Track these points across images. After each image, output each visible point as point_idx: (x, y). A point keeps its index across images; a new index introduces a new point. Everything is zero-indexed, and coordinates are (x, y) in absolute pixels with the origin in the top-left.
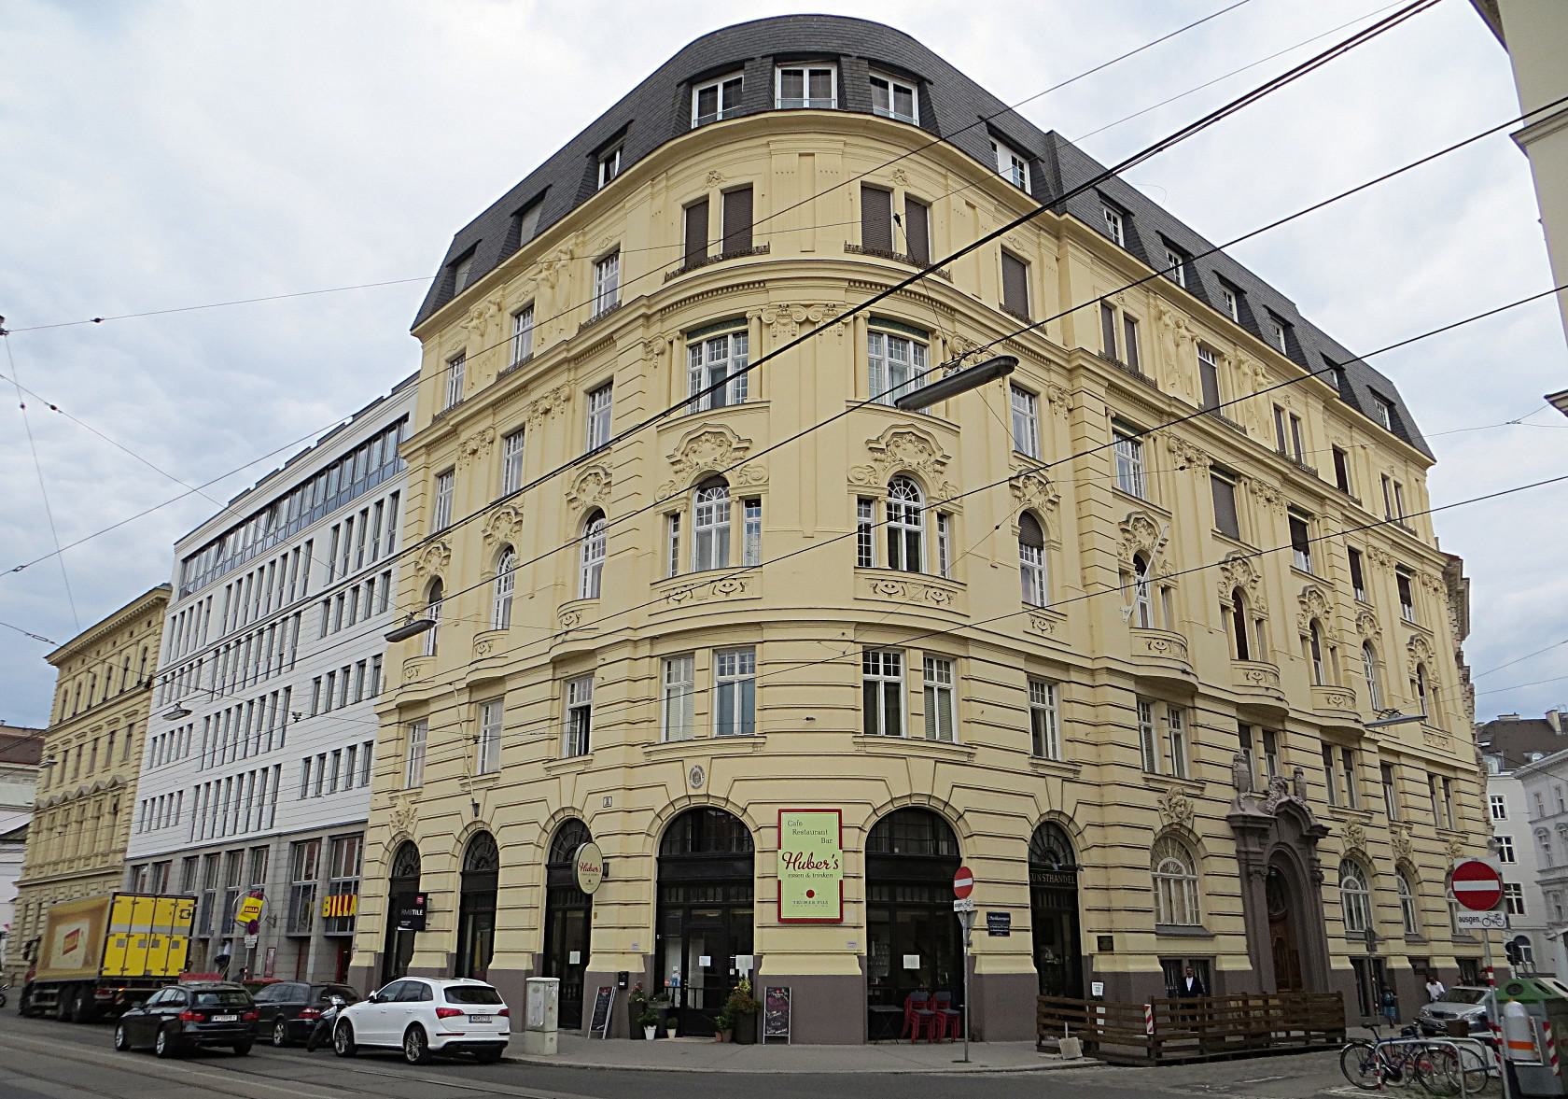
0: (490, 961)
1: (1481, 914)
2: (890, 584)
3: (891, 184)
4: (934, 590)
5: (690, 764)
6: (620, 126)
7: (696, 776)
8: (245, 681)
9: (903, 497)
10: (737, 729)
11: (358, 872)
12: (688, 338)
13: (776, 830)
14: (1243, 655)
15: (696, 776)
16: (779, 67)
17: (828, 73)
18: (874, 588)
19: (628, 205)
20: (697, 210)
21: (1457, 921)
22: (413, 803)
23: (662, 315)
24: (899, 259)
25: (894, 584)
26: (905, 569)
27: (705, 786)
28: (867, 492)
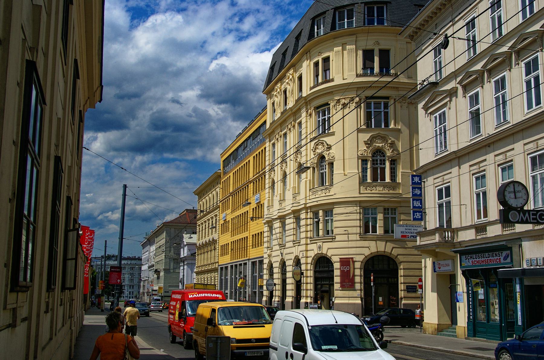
0: (285, 299)
6: (285, 49)
7: (320, 247)
8: (306, 197)
9: (379, 157)
11: (263, 272)
12: (317, 109)
13: (74, 261)
15: (320, 247)
19: (334, 42)
20: (316, 64)
22: (271, 251)
23: (309, 102)
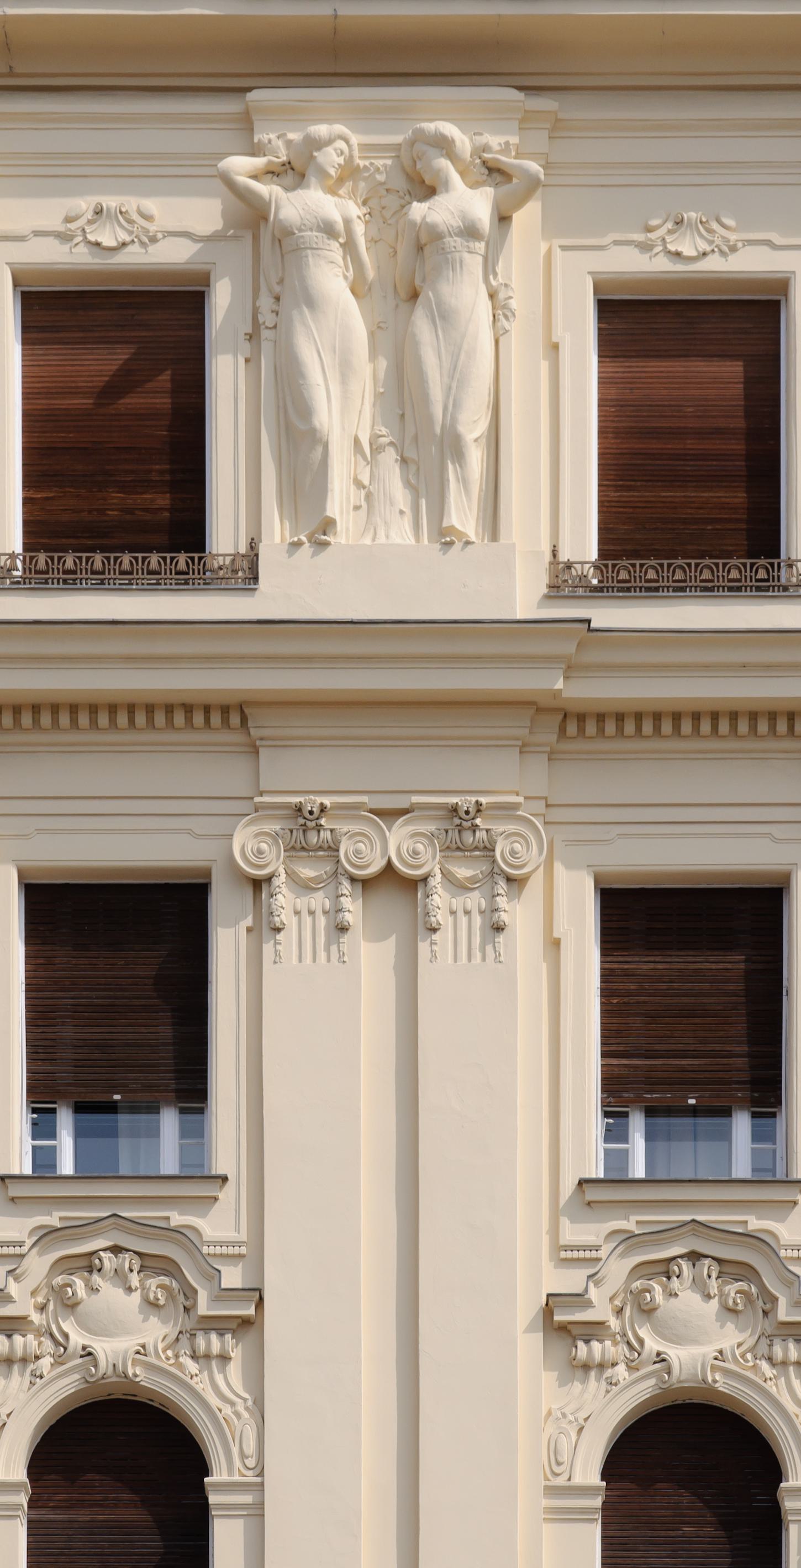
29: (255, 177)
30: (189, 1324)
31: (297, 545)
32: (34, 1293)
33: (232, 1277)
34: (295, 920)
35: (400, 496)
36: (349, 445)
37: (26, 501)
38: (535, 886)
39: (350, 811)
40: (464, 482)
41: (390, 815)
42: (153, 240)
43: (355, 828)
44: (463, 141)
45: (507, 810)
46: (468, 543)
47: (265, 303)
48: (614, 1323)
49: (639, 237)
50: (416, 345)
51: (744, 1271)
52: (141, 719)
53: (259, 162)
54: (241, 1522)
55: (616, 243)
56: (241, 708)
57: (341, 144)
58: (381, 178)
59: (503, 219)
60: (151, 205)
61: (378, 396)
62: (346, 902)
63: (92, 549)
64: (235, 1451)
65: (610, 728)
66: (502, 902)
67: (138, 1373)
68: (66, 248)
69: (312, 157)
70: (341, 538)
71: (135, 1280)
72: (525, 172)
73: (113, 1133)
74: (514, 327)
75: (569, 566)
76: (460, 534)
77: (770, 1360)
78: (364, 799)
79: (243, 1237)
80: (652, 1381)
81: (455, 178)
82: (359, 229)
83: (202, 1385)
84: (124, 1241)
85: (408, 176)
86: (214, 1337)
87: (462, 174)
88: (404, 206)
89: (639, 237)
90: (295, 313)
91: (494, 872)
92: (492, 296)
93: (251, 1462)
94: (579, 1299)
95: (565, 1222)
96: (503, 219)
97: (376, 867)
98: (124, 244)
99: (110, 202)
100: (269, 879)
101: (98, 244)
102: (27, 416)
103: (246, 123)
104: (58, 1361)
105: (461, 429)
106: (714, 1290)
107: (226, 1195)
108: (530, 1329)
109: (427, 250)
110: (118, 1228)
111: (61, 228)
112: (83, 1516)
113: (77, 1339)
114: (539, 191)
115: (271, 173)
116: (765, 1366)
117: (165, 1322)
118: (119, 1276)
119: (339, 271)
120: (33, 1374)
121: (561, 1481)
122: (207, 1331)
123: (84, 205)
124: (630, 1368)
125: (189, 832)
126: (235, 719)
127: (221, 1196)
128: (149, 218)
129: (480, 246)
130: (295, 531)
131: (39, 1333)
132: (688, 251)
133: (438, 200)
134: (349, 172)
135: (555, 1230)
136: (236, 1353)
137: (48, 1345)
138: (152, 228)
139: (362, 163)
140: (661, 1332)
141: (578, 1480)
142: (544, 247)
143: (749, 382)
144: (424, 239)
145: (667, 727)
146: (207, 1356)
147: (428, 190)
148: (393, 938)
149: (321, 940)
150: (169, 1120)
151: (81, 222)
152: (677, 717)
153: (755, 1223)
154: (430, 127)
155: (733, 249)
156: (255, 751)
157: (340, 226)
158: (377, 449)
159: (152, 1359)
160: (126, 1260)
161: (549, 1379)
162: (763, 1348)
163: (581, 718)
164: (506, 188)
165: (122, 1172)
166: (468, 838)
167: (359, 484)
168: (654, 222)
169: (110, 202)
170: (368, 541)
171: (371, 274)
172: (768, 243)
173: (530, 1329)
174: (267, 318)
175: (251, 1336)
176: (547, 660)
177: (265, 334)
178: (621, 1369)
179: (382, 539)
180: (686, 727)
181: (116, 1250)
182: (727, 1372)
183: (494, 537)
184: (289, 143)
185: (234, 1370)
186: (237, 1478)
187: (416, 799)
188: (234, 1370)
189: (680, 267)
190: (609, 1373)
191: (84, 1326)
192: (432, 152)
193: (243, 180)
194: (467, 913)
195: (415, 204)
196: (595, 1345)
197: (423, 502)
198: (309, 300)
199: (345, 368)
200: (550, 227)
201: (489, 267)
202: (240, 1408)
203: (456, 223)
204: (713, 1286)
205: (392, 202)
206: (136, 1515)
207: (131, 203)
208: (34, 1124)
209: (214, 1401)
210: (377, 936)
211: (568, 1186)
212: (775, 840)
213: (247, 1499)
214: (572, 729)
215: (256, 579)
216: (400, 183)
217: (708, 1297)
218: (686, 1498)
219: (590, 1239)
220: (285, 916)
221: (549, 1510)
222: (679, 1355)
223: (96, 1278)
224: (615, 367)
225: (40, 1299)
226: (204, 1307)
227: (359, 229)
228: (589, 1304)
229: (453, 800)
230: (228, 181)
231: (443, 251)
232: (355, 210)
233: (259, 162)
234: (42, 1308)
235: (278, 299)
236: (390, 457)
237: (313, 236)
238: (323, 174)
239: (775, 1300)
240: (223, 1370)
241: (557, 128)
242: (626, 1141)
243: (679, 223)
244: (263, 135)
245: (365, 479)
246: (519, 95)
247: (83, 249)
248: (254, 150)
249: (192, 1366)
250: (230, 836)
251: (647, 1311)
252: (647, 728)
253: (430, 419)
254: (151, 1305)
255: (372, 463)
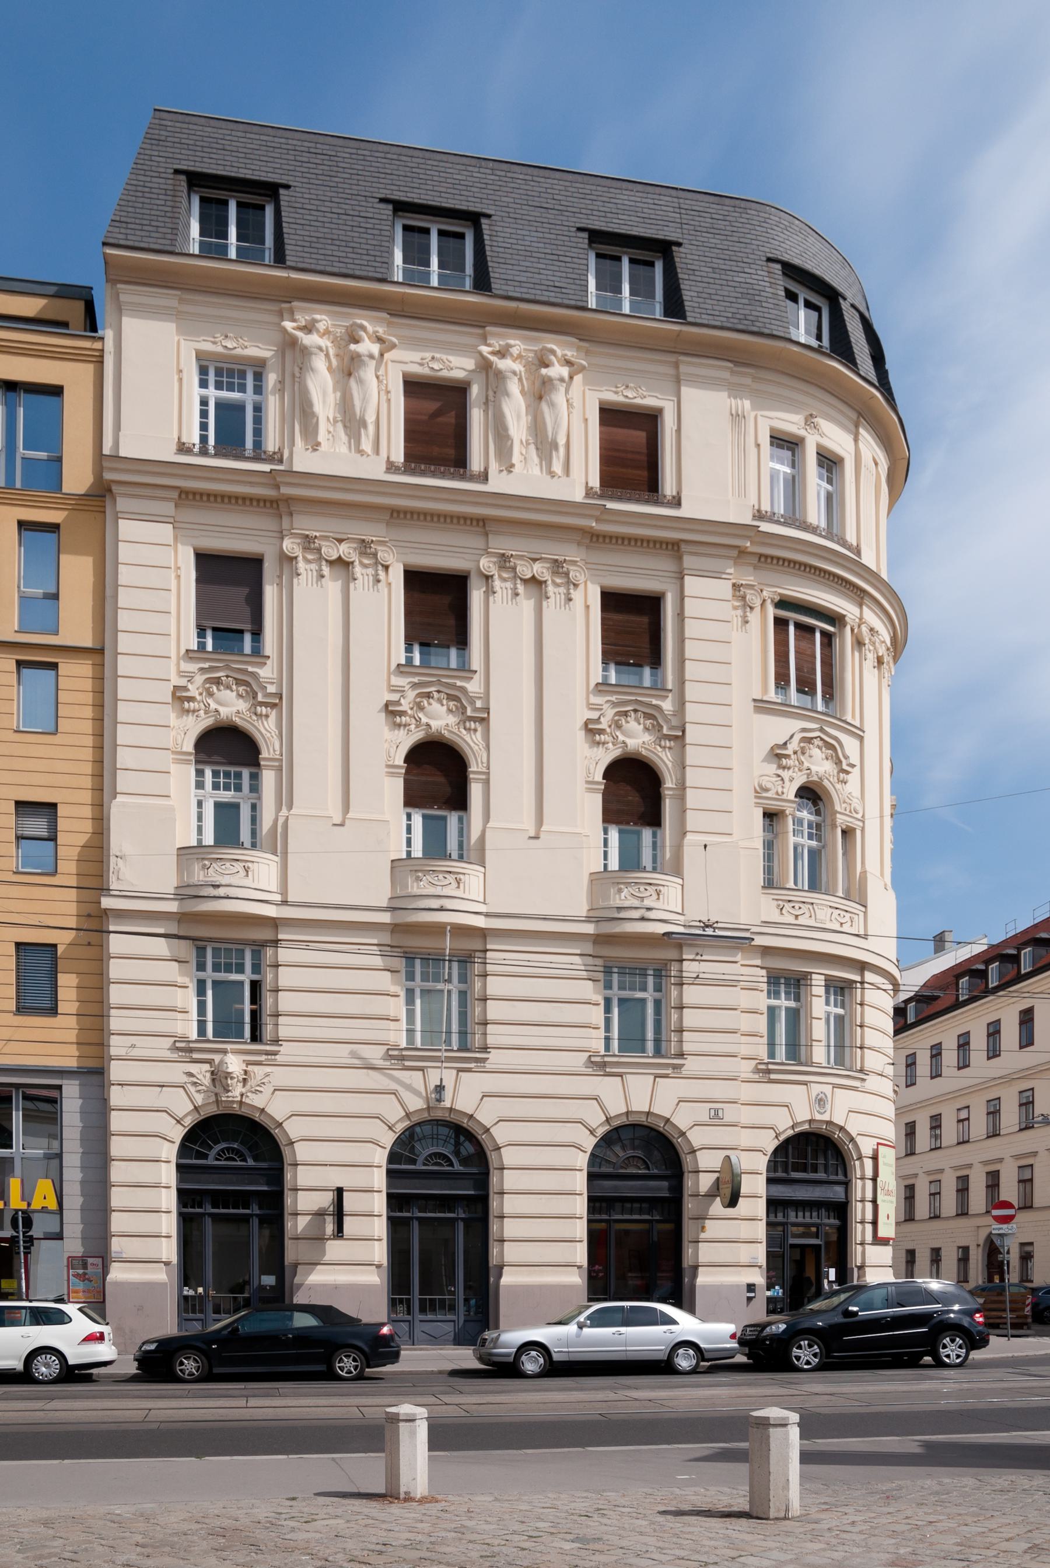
1: (1005, 1226)
2: (797, 906)
3: (802, 433)
4: (838, 912)
5: (816, 1089)
10: (819, 1054)
14: (187, 962)
15: (821, 1101)
16: (196, 192)
17: (461, 236)
18: (782, 909)
21: (100, 1266)
24: (813, 530)
25: (801, 905)
26: (806, 888)
27: (828, 1112)
28: (774, 805)
29: (294, 329)
30: (463, 718)
31: (502, 471)
32: (198, 689)
33: (479, 704)
34: (361, 577)
35: (536, 460)
36: (519, 441)
37: (405, 447)
38: (581, 587)
39: (521, 557)
40: (367, 435)
41: (535, 560)
42: (452, 369)
43: (522, 562)
44: (370, 328)
45: (574, 563)
46: (368, 455)
47: (491, 393)
48: (608, 730)
49: (614, 389)
50: (350, 389)
51: (651, 717)
52: (448, 520)
53: (490, 349)
54: (273, 772)
55: (204, 340)
56: (483, 520)
57: (518, 347)
58: (530, 359)
59: (571, 378)
60: (451, 358)
61: (528, 428)
62: (519, 586)
63: (441, 465)
64: (479, 761)
65: (607, 540)
66: (572, 591)
67: (446, 734)
68: (421, 368)
69: (508, 350)
70: (516, 470)
71: (445, 702)
72: (391, 341)
73: (429, 654)
74: (575, 411)
75: (592, 488)
76: (366, 453)
77: (660, 746)
78: (331, 534)
79: (482, 691)
80: (621, 750)
81: (556, 362)
82: (523, 374)
83: (467, 738)
84: (442, 689)
85: (349, 336)
86: (472, 723)
87: (558, 362)
88: (348, 345)
89: (614, 389)
90: (502, 399)
91: (377, 563)
92: (567, 401)
93: (485, 765)
94: (398, 703)
95: (392, 677)
96: (571, 378)
97: (334, 557)
98: (441, 369)
99: (437, 355)
100: (492, 576)
101: (432, 368)
102: (408, 421)
103: (292, 312)
104: (417, 727)
105: (367, 418)
106: (642, 722)
107: (476, 677)
108: (580, 729)
109: (355, 360)
110: (439, 684)
111: (420, 361)
112: (424, 778)
113: (424, 720)
114: (585, 372)
115: (300, 328)
116: (658, 747)
117: (455, 716)
118: (440, 701)
119: (517, 386)
120: (408, 730)
121: (590, 779)
122: (470, 721)
123: (428, 355)
124: (614, 745)
125: (464, 558)
126: (481, 524)
127: (268, 662)
128: (450, 362)
129: (565, 385)
130: (500, 466)
131: (410, 717)
132: (630, 396)
133: (359, 344)
134: (327, 332)
135: (588, 698)
136: (479, 729)
137: (413, 721)
138: (452, 365)
139: (524, 354)
140: (624, 734)
141: (396, 763)
142: (176, 339)
143: (648, 439)
144: (546, 380)
145: (620, 542)
146: (261, 715)
147: (357, 341)
148: (340, 582)
149: (315, 580)
150: (453, 652)
151: (427, 360)
152: (642, 541)
153: (655, 702)
154: (359, 321)
155: (645, 397)
156: (486, 534)
157: (324, 349)
158: (528, 444)
159: (450, 729)
160: (442, 695)
161: (587, 746)
162: (253, 710)
163: (598, 536)
164: (572, 368)
165: (432, 665)
166: (368, 551)
167: (522, 454)
168: (216, 336)
169: (437, 355)
170: (525, 472)
171: (526, 389)
172: (656, 397)
173: (580, 729)
174: (491, 398)
175: (485, 724)
176: (591, 516)
177: (490, 403)
178: (610, 745)
179: (530, 472)
180: (633, 543)
181: (439, 692)
182: (646, 748)
183: (568, 475)
184: (500, 345)
185: (479, 734)
186: (480, 770)
187: (349, 536)
188: (479, 734)
189: (627, 400)
190: (606, 745)
191: (426, 715)
192: (358, 329)
193: (485, 354)
194: (367, 575)
195: (352, 345)
196: (602, 736)
197: (352, 441)
198: (508, 395)
199: (519, 417)
200: (586, 382)
201: (567, 391)
202: (273, 734)
203: (366, 353)
204: (642, 720)
205: (534, 368)
206: (442, 780)
207: (444, 357)
208: (406, 648)
209: (472, 744)
210: (336, 580)
211: (393, 666)
212: (661, 582)
213: (484, 777)
214: (594, 539)
215: (487, 480)
216: (347, 338)
217: (640, 724)
218: (629, 788)
219: (600, 702)
220: (497, 588)
221: (586, 788)
222: (629, 741)
223: (431, 700)
224: (605, 428)
225: (411, 706)
226: (469, 713)
227: (523, 374)
228: (188, 690)
229: (307, 533)
230: (480, 353)
231: (553, 384)
232: (329, 344)
233: (294, 324)
234: (412, 709)
235: (301, 369)
236: (532, 447)
237: (510, 374)
238: (512, 355)
239: (662, 727)
240: (475, 734)
241: (587, 353)
242: (205, 638)
243: (627, 387)
244: (490, 341)
245: (524, 453)
246: (388, 316)
247: (427, 369)
248: (294, 321)
249: (464, 732)
250: (479, 561)
251: (619, 727)
252: (645, 544)
253: (355, 414)
254: (450, 711)
255: (526, 448)
